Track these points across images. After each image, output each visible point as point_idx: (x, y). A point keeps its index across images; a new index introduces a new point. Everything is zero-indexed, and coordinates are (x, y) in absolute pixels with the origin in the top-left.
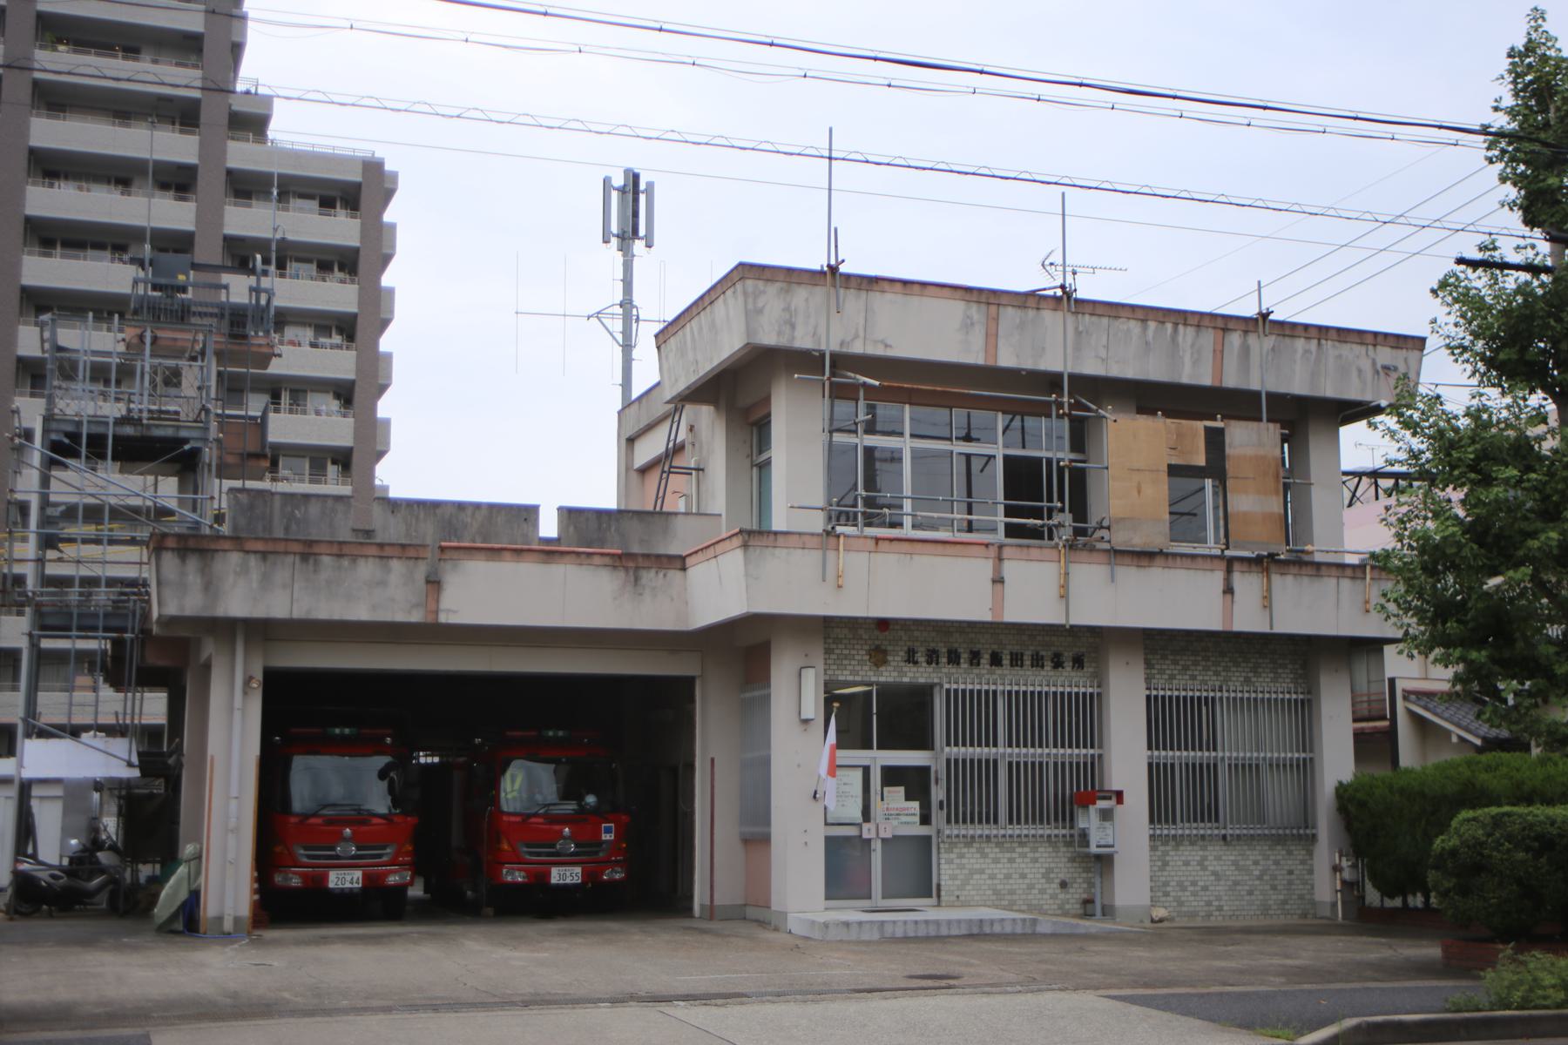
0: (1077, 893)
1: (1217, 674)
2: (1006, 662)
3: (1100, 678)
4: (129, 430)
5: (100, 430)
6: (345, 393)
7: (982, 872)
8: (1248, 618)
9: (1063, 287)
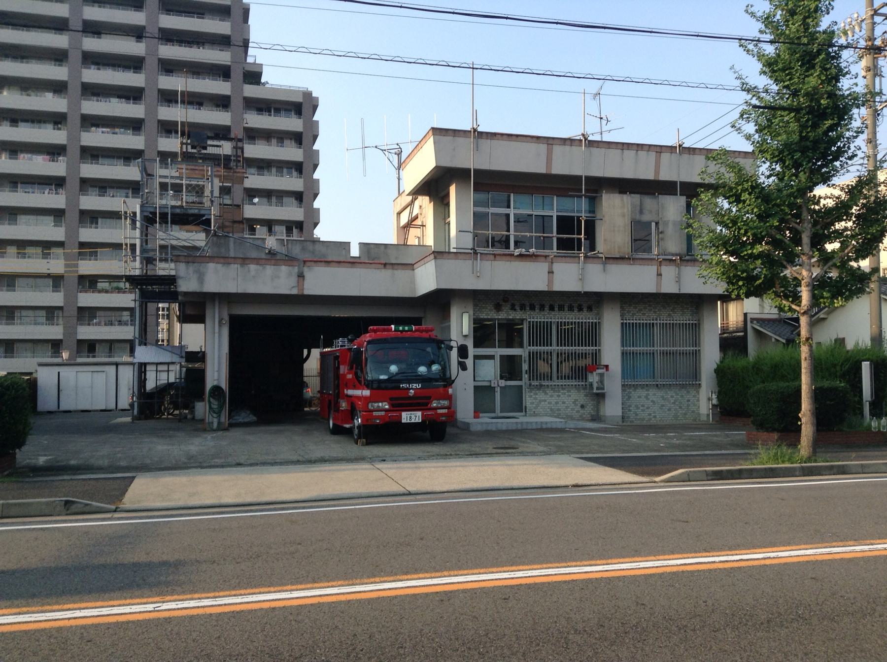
0: (589, 410)
1: (655, 312)
2: (556, 309)
3: (599, 316)
4: (178, 211)
5: (166, 210)
6: (299, 196)
7: (545, 401)
8: (669, 287)
9: (583, 135)
